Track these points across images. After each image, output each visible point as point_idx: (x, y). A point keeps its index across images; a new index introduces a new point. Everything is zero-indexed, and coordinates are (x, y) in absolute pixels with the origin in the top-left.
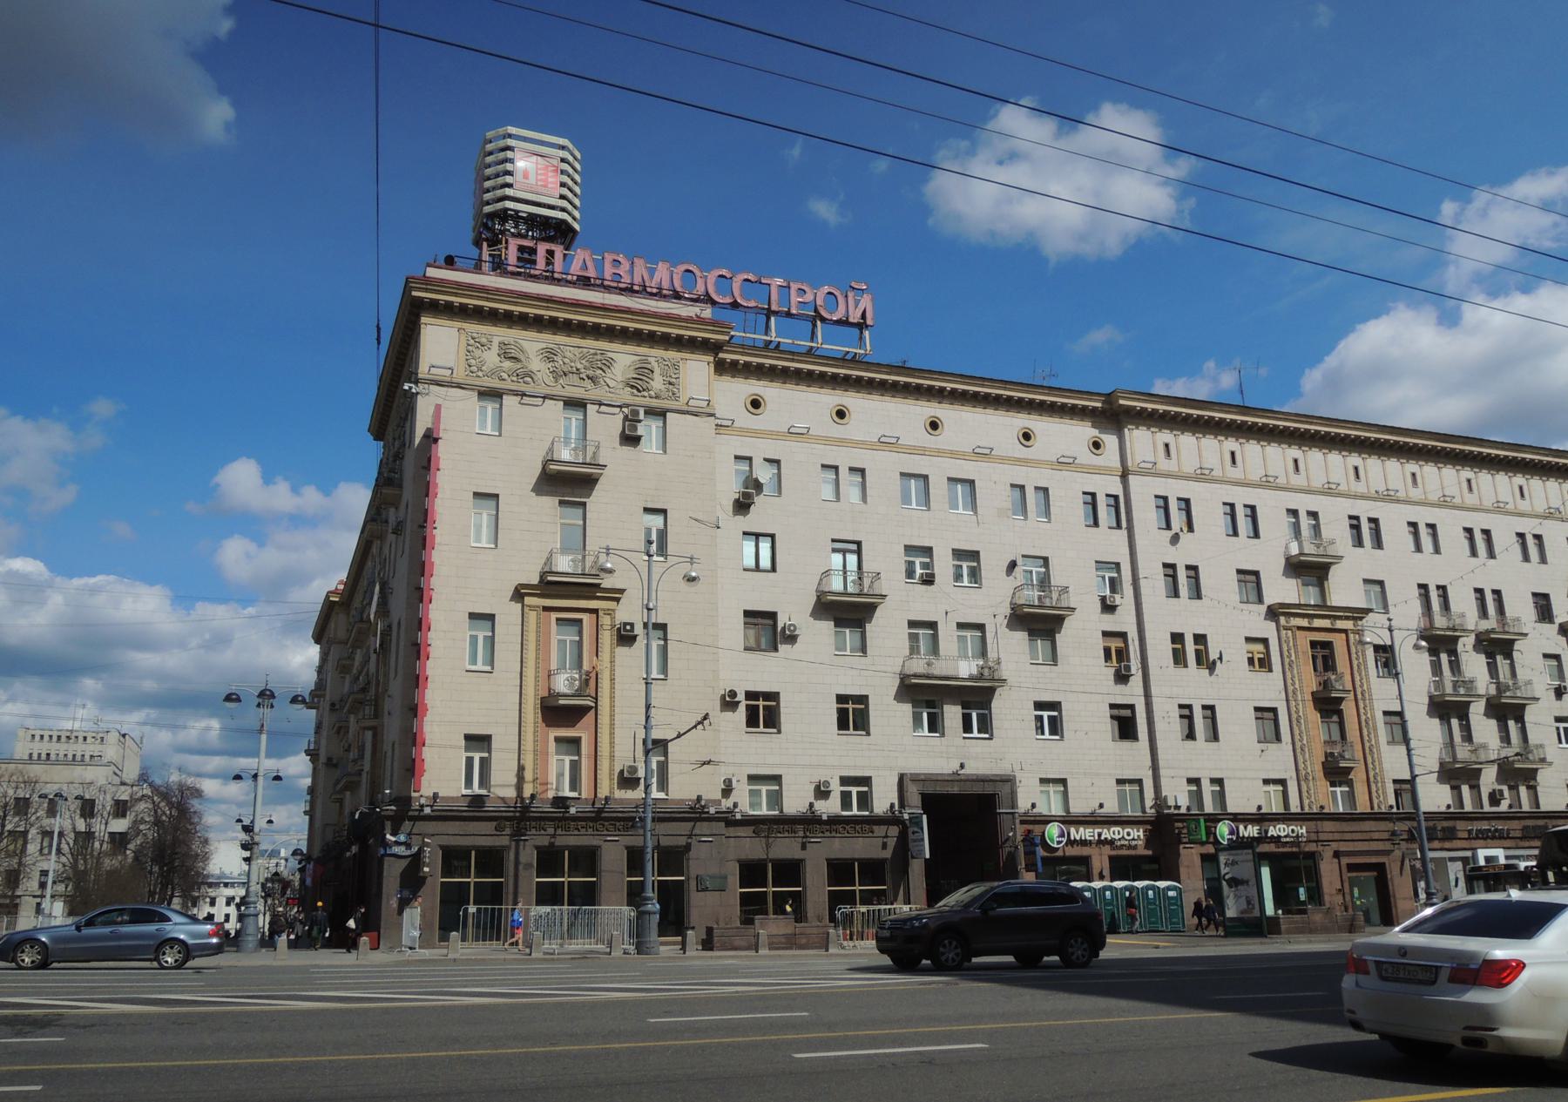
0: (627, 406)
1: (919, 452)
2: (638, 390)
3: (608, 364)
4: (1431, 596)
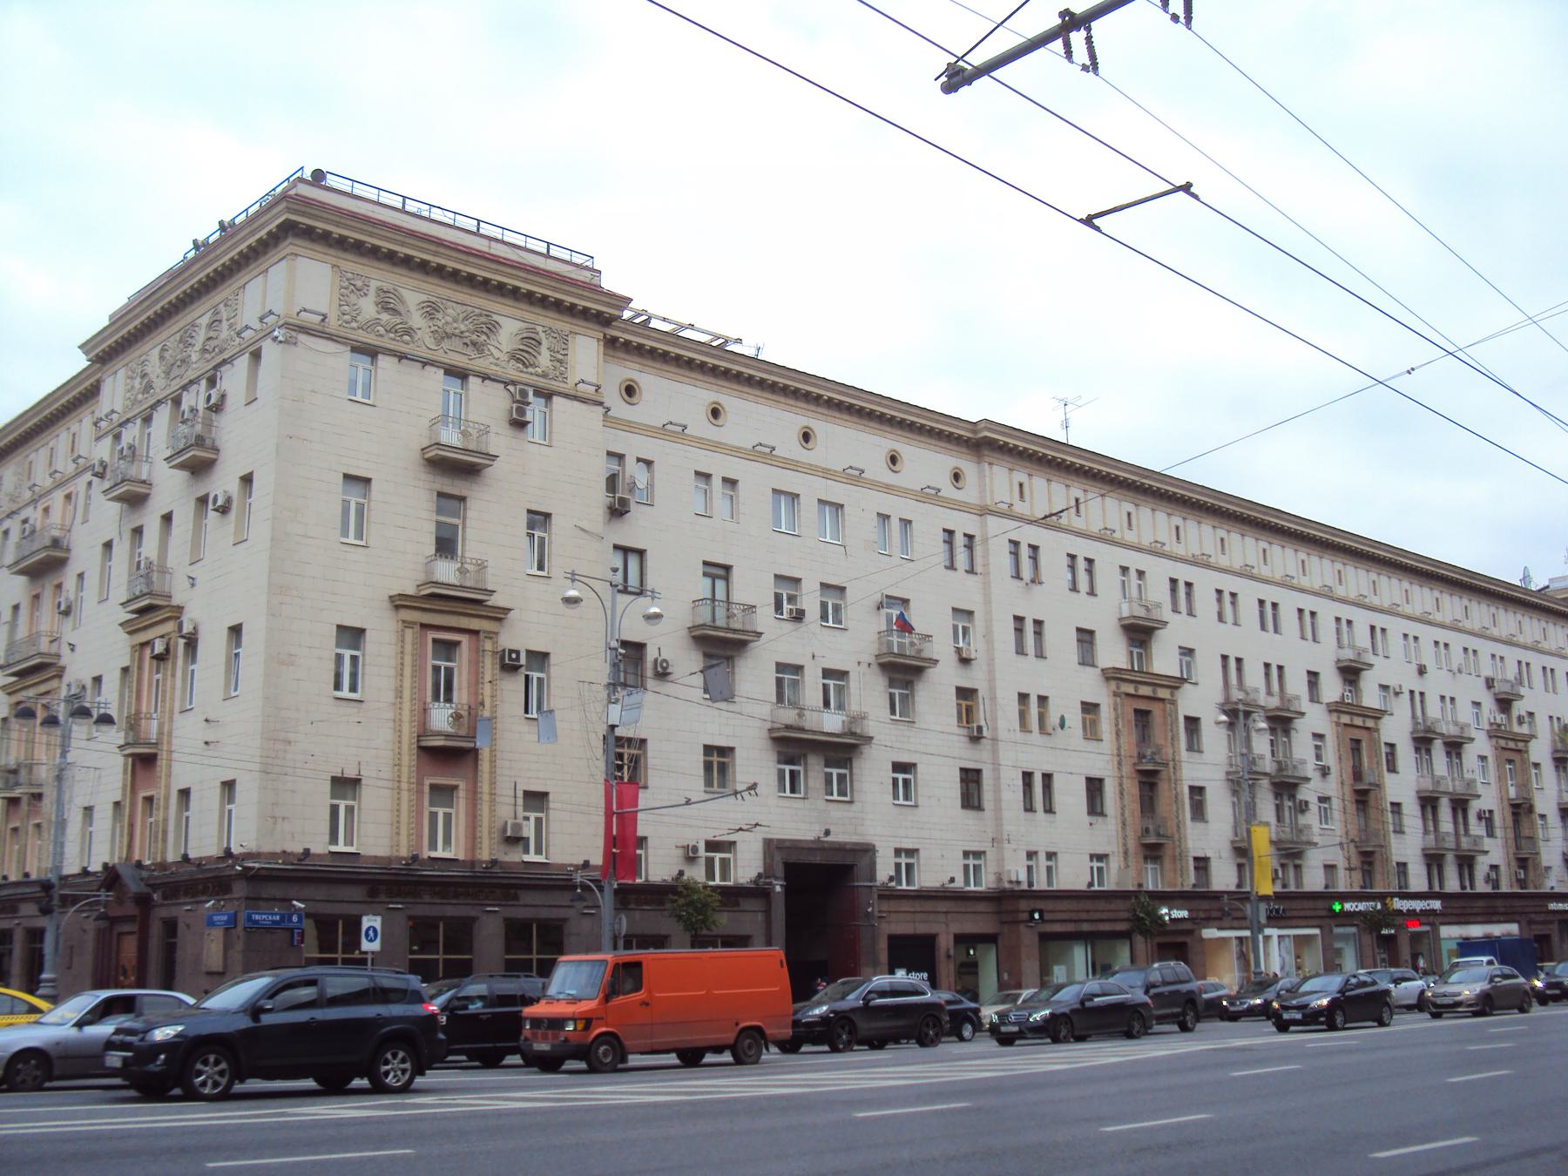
0: (514, 383)
1: (805, 470)
2: (524, 364)
3: (492, 328)
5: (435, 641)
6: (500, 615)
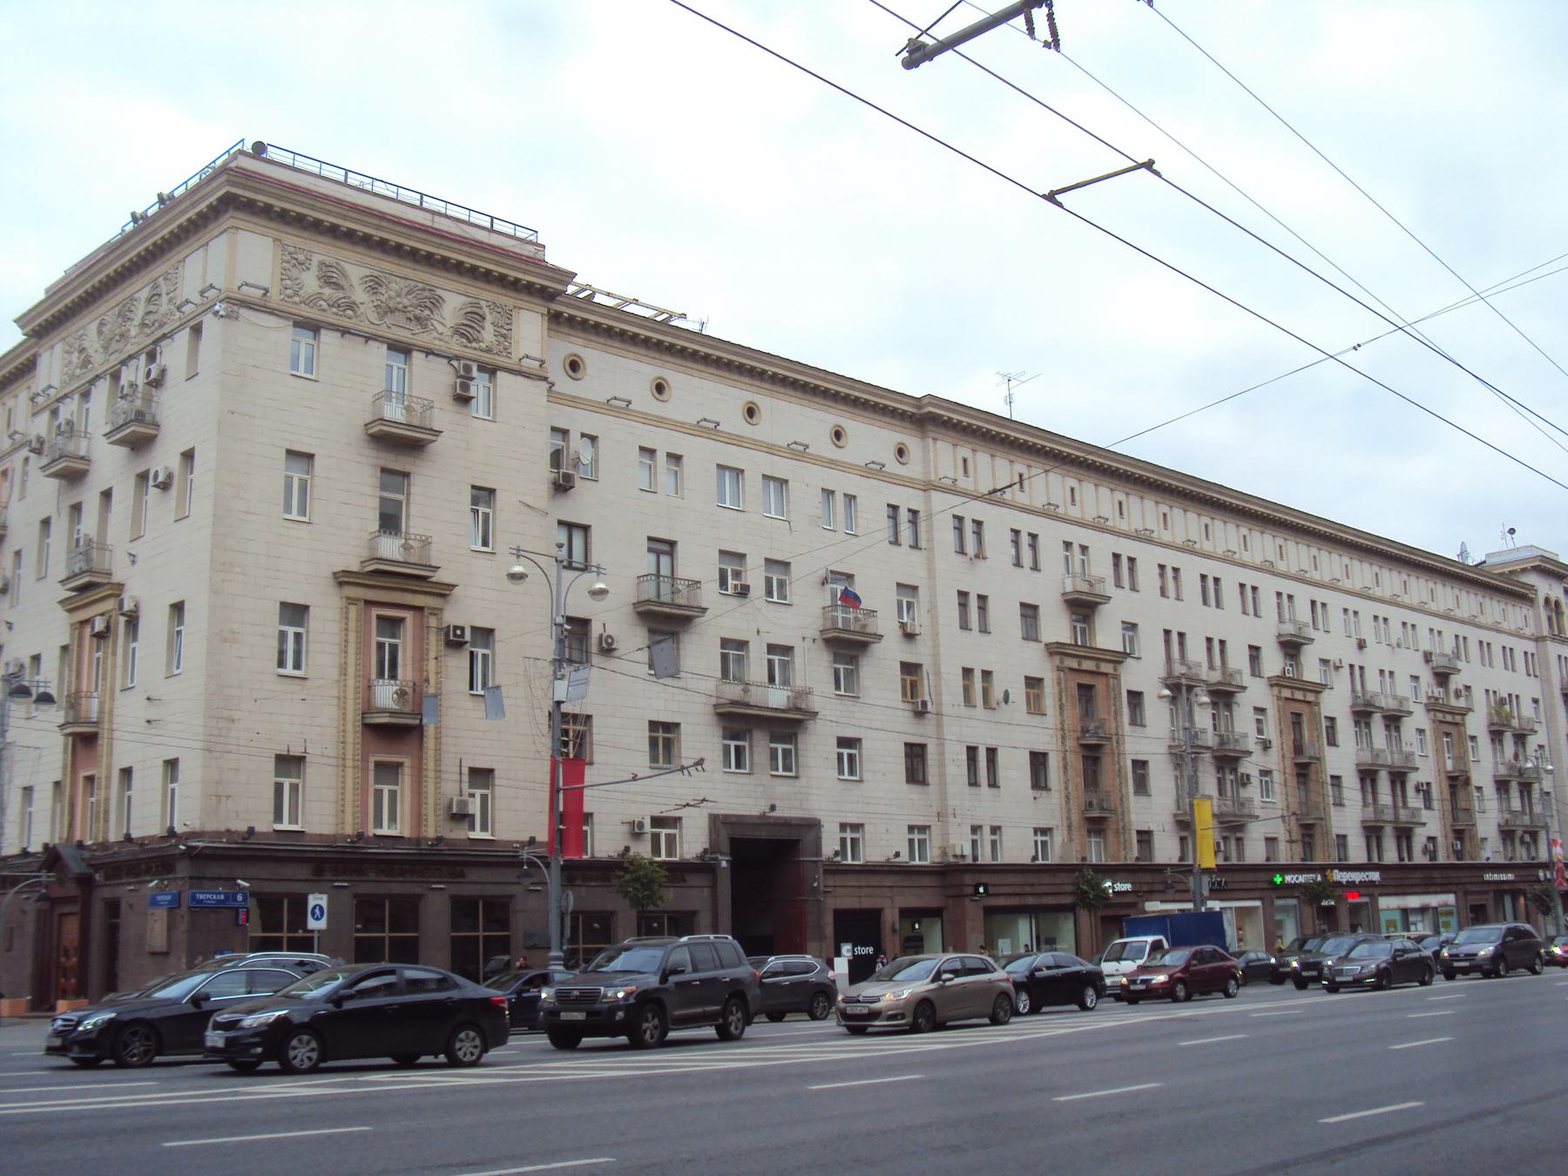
0: (458, 358)
2: (468, 339)
3: (435, 303)
4: (1174, 639)
5: (379, 617)
6: (444, 591)
